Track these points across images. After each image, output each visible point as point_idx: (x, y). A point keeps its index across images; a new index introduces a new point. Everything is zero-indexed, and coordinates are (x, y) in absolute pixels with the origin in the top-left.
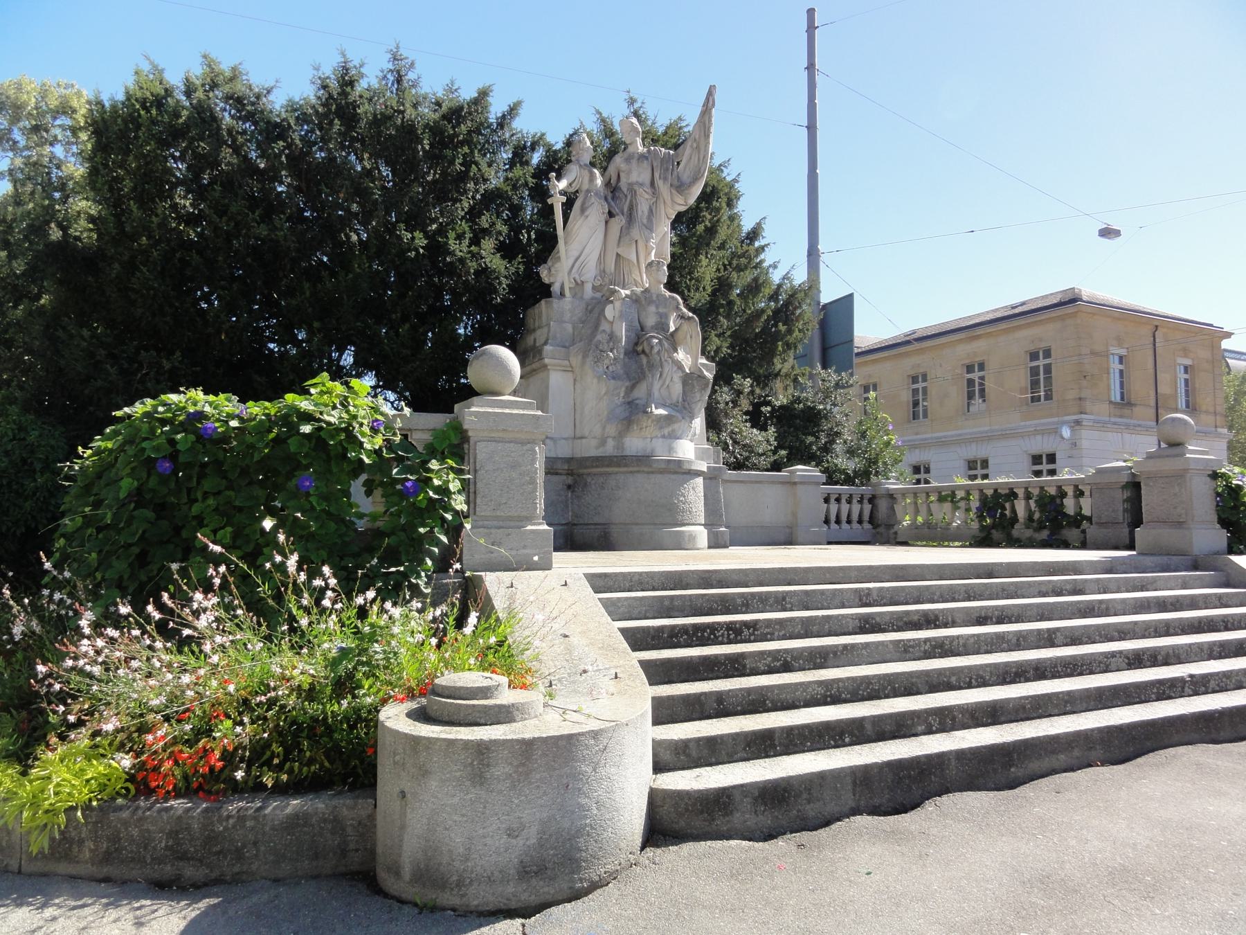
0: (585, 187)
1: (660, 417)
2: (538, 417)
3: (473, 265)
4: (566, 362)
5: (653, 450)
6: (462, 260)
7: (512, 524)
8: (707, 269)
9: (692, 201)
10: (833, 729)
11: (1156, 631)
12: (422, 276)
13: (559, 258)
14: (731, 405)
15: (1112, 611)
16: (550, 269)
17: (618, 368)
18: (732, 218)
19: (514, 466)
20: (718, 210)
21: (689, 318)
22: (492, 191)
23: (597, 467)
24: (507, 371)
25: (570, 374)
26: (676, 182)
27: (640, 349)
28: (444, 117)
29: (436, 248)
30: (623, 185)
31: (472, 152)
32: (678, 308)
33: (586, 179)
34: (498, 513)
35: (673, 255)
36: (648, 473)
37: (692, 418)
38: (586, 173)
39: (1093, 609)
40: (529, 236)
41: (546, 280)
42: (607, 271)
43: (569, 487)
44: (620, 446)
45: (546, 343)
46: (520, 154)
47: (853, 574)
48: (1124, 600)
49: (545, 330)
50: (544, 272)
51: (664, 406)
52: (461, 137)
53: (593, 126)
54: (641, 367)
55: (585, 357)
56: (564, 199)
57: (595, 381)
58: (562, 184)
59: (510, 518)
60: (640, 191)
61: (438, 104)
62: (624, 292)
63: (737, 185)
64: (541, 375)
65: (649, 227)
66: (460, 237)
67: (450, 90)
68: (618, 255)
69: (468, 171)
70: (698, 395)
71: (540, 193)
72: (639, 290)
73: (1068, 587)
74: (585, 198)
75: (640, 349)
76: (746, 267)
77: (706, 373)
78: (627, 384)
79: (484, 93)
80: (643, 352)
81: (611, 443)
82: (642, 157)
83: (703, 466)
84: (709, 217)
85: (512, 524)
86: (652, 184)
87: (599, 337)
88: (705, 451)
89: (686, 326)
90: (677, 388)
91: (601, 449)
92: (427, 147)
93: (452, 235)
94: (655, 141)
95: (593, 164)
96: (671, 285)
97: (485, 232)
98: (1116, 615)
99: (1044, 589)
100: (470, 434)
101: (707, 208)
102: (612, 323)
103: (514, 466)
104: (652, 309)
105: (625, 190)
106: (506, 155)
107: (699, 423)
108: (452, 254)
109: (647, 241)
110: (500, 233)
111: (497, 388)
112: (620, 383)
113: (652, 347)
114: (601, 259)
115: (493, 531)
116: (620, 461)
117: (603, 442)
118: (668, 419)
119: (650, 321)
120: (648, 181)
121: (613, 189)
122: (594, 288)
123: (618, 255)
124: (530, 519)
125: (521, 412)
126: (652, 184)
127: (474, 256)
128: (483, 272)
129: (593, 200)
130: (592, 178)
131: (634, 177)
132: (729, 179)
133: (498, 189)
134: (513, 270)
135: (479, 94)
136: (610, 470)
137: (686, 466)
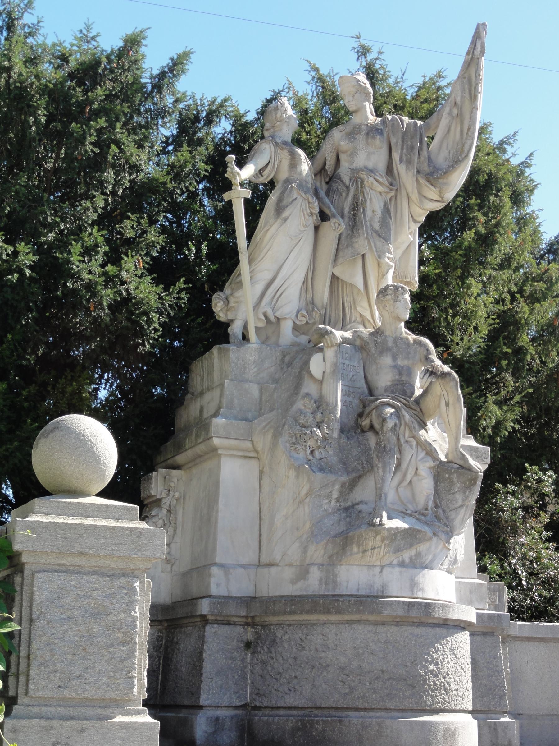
0: (283, 175)
1: (396, 533)
2: (140, 533)
3: (107, 295)
4: (248, 444)
5: (384, 587)
6: (90, 286)
7: (89, 712)
8: (480, 300)
9: (450, 195)
12: (30, 310)
13: (241, 282)
14: (520, 513)
16: (227, 300)
17: (330, 455)
18: (522, 223)
19: (96, 614)
20: (497, 209)
21: (444, 375)
22: (143, 185)
23: (293, 613)
24: (92, 456)
25: (254, 463)
26: (425, 168)
27: (365, 423)
28: (71, 76)
29: (52, 269)
30: (344, 172)
31: (112, 126)
32: (427, 359)
33: (286, 163)
34: (67, 693)
35: (424, 279)
36: (376, 624)
37: (450, 534)
38: (285, 156)
40: (199, 250)
41: (221, 315)
42: (317, 300)
43: (248, 645)
44: (330, 578)
45: (216, 414)
46: (190, 127)
49: (216, 393)
50: (218, 306)
51: (403, 515)
52: (95, 106)
53: (306, 88)
54: (366, 451)
55: (276, 436)
56: (248, 193)
57: (292, 473)
58: (248, 172)
59: (87, 703)
60: (369, 181)
61: (64, 58)
62: (339, 334)
63: (528, 171)
64: (208, 465)
65: (384, 234)
66: (88, 252)
67: (85, 37)
68: (334, 278)
69: (103, 154)
70: (459, 497)
71: (220, 183)
72: (365, 331)
74: (283, 192)
75: (365, 423)
76: (545, 297)
77: (472, 462)
78: (344, 478)
79: (133, 42)
80: (372, 427)
81: (315, 574)
82: (373, 131)
83: (469, 614)
84: (483, 219)
85: (89, 712)
86: (389, 169)
87: (300, 404)
88: (474, 589)
89: (438, 387)
90: (425, 486)
91: (300, 584)
92: (43, 120)
93: (76, 248)
94: (398, 108)
95: (298, 142)
96: (420, 323)
97: (131, 244)
100: (24, 559)
101: (480, 207)
102: (321, 382)
103: (96, 614)
104: (387, 360)
105: (346, 179)
106: (167, 129)
107: (463, 542)
108: (76, 277)
109: (380, 256)
110: (151, 246)
111: (77, 484)
112: (331, 477)
113: (384, 420)
114: (308, 283)
115: (56, 723)
116: (331, 603)
117: (303, 572)
118: (410, 537)
119: (384, 379)
120: (382, 165)
121: (328, 178)
122: (296, 328)
123: (334, 278)
124: (120, 704)
125: (113, 523)
126: (389, 169)
127: (109, 280)
128: (125, 304)
129: (295, 195)
130: (294, 163)
131: (361, 160)
132: (515, 161)
133: (151, 181)
134: (170, 300)
135: (126, 41)
136: (313, 618)
137: (439, 614)
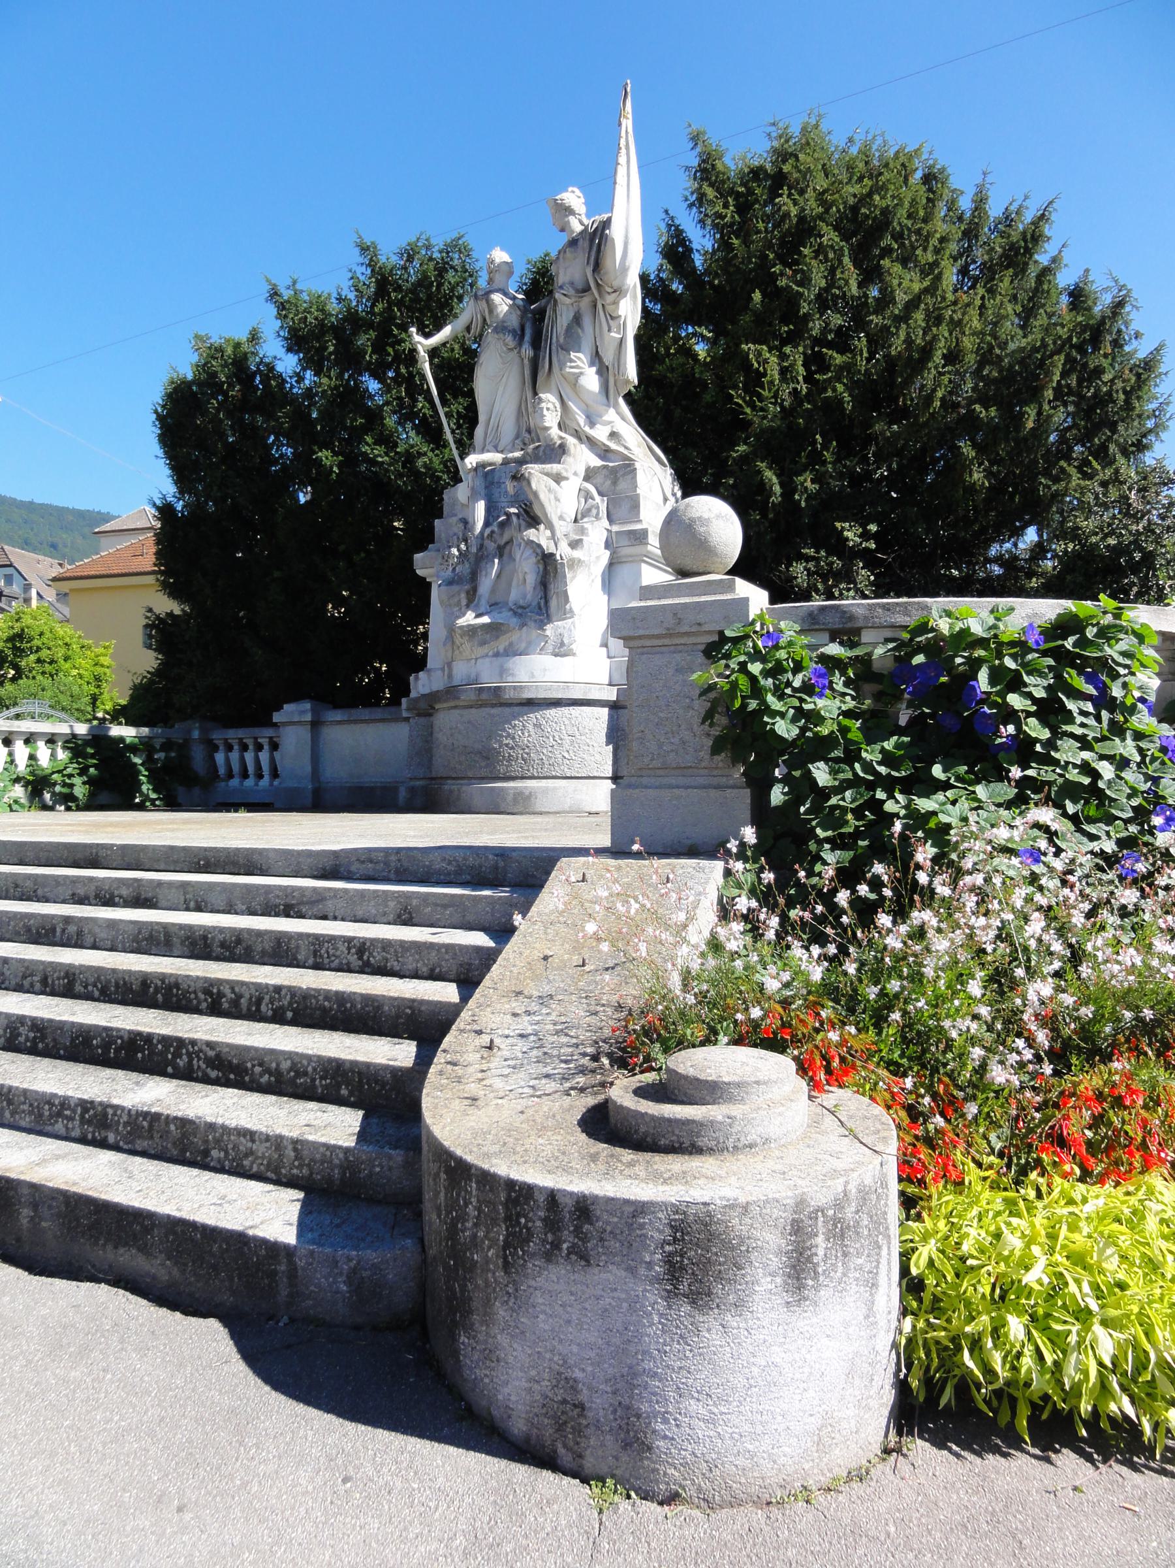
10: (345, 1074)
11: (44, 981)
15: (89, 940)
39: (54, 930)
47: (31, 855)
48: (112, 924)
73: (125, 892)
98: (95, 947)
99: (81, 891)
